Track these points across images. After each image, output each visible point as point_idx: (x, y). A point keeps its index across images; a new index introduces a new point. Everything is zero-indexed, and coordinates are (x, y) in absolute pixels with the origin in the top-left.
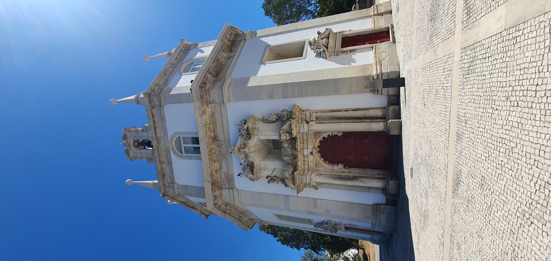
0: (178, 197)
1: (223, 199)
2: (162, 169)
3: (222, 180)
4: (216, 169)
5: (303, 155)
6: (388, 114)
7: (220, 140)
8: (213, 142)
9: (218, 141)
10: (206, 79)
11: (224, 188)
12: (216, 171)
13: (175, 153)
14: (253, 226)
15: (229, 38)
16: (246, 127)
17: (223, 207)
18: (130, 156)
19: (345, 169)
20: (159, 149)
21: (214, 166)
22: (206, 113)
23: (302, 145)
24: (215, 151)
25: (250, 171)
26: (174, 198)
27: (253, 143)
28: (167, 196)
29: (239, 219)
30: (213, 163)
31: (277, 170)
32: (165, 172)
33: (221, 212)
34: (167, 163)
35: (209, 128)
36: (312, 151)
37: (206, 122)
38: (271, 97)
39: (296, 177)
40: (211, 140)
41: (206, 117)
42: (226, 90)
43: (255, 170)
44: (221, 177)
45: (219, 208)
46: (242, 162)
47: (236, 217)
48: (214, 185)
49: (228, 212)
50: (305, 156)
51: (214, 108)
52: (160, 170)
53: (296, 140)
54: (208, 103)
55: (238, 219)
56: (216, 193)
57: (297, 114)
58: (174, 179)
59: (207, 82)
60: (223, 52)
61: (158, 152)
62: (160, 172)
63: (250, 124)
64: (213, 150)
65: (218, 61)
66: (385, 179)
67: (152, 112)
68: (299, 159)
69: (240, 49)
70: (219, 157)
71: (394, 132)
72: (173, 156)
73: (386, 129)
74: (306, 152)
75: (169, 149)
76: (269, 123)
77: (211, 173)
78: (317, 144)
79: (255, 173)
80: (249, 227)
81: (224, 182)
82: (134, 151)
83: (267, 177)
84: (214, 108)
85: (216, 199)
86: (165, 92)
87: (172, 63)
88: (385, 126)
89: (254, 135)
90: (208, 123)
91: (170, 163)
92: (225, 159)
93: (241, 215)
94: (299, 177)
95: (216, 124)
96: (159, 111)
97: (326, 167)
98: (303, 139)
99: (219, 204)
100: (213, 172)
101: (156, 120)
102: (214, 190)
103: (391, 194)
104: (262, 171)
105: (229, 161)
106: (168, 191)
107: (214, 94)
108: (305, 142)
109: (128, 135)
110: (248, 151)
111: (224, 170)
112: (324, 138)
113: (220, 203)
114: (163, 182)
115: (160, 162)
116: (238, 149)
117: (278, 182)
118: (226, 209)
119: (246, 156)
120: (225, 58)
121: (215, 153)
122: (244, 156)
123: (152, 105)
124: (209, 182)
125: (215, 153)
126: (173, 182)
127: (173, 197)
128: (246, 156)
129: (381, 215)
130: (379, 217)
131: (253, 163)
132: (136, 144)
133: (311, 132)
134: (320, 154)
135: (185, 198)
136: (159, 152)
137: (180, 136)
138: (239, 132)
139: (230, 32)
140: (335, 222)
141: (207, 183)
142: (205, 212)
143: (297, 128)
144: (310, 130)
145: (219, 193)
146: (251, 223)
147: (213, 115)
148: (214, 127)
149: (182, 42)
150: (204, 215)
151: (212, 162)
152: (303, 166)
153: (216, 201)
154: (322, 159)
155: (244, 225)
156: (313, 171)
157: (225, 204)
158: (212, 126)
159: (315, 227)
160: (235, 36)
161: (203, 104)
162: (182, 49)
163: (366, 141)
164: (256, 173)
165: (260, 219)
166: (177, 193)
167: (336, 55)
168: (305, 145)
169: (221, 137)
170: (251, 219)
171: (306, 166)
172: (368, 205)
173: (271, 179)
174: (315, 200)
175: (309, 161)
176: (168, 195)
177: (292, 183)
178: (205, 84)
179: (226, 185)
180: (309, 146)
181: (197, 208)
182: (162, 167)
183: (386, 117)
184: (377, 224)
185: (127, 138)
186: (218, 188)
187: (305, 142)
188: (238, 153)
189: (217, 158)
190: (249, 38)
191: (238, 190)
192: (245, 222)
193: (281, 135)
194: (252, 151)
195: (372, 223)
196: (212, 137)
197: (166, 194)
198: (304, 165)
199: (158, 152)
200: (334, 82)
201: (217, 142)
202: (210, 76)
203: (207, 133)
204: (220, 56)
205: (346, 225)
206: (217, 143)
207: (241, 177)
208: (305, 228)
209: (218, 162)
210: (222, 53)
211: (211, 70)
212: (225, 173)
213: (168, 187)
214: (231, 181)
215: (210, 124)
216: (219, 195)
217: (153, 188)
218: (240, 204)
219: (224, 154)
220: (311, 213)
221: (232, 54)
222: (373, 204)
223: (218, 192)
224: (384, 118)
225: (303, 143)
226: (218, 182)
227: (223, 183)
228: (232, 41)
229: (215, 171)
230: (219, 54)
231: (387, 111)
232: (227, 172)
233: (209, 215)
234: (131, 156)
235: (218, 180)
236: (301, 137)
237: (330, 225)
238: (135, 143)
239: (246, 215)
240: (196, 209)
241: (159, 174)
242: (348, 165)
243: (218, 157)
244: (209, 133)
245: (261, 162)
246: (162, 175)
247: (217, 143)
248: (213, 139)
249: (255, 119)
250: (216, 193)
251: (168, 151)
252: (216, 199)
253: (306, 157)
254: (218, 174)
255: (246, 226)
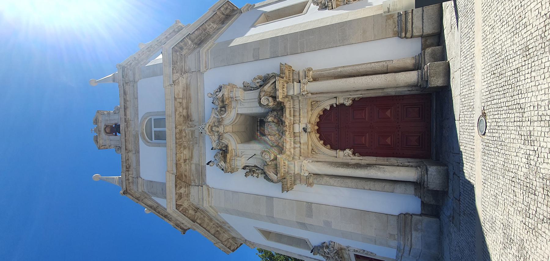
0: (145, 198)
1: (191, 200)
2: (128, 160)
3: (192, 174)
4: (185, 157)
5: (293, 133)
6: (423, 61)
7: (193, 119)
8: (185, 122)
9: (191, 121)
10: (184, 44)
11: (193, 185)
12: (185, 161)
13: (144, 138)
14: (237, 249)
15: (223, 12)
16: (220, 95)
17: (191, 212)
18: (99, 143)
19: (355, 156)
20: (127, 134)
21: (182, 154)
22: (179, 84)
23: (292, 118)
24: (186, 134)
25: (222, 158)
26: (139, 199)
27: (230, 116)
28: (130, 194)
29: (216, 235)
30: (182, 149)
31: (258, 157)
32: (130, 163)
33: (187, 218)
34: (134, 152)
35: (180, 103)
36: (306, 126)
37: (178, 94)
38: (257, 59)
39: (279, 163)
40: (182, 119)
41: (179, 89)
42: (204, 53)
43: (228, 156)
44: (190, 169)
45: (184, 212)
46: (214, 145)
47: (211, 231)
48: (180, 180)
49: (198, 221)
50: (295, 135)
51: (189, 79)
52: (125, 160)
53: (284, 110)
54: (184, 72)
55: (215, 234)
56: (182, 191)
57: (287, 73)
58: (139, 173)
59: (185, 48)
60: (213, 23)
61: (125, 137)
62: (125, 162)
63: (225, 92)
64: (184, 133)
65: (205, 30)
66: (420, 167)
67: (124, 88)
68: (288, 139)
69: (233, 20)
70: (191, 142)
71: (437, 82)
72: (141, 142)
73: (422, 78)
74: (298, 128)
75: (138, 134)
76: (251, 90)
77: (178, 163)
78: (315, 119)
79: (229, 161)
80: (230, 249)
81: (193, 176)
82: (104, 138)
83: (244, 168)
84: (190, 78)
85: (181, 198)
86: (141, 65)
87: (160, 41)
88: (420, 74)
89: (231, 107)
90: (181, 96)
91: (137, 152)
92: (197, 145)
93: (218, 229)
94: (284, 163)
95: (190, 99)
96: (133, 87)
97: (327, 152)
98: (294, 110)
99: (184, 206)
100: (181, 161)
101: (128, 99)
102: (178, 186)
103: (432, 190)
104: (238, 158)
105: (201, 147)
106: (131, 188)
107: (191, 62)
108: (297, 114)
109: (100, 119)
110: (222, 130)
111: (195, 160)
112: (325, 111)
113: (186, 205)
114: (126, 176)
115: (126, 149)
116: (210, 127)
117: (258, 175)
118: (196, 217)
119: (220, 137)
120: (215, 29)
121: (185, 137)
122: (217, 137)
123: (126, 80)
124: (173, 174)
125: (185, 137)
126: (138, 176)
127: (138, 197)
128: (220, 137)
129: (413, 232)
130: (409, 237)
131: (227, 146)
132: (108, 130)
133: (303, 93)
134: (318, 135)
135: (153, 200)
136: (126, 138)
137: (151, 118)
138: (212, 103)
139: (225, 6)
140: (341, 245)
141: (171, 174)
142: (182, 225)
143: (285, 89)
144: (302, 90)
145: (185, 191)
146: (234, 243)
147: (187, 87)
148: (187, 103)
149: (176, 23)
150: (180, 228)
151: (180, 148)
152: (292, 151)
153: (180, 201)
154: (322, 142)
155: (223, 245)
156: (307, 157)
157: (194, 208)
158: (184, 101)
159: (311, 252)
160: (231, 11)
161: (175, 71)
162: (176, 30)
163: (388, 113)
164: (230, 160)
165: (244, 238)
166: (140, 190)
167: (345, 3)
168: (297, 118)
169: (195, 117)
170: (234, 238)
171: (296, 149)
172: (392, 215)
173: (250, 170)
174: (309, 205)
175: (302, 142)
176: (132, 194)
177: (274, 172)
178: (181, 48)
179: (196, 181)
180: (302, 119)
181: (171, 218)
182: (128, 156)
183: (420, 65)
184: (407, 248)
185: (98, 122)
186: (186, 183)
187: (297, 114)
188: (209, 132)
189: (188, 144)
190: (245, 10)
191: (209, 187)
192: (224, 240)
193: (260, 99)
194: (228, 130)
195: (398, 249)
196: (183, 116)
197: (129, 192)
198: (294, 148)
199: (125, 137)
200: (341, 28)
201: (190, 123)
202: (190, 42)
203: (177, 109)
204: (209, 26)
205: (357, 251)
206: (189, 124)
207: (211, 166)
208: (300, 255)
209: (189, 148)
210: (212, 24)
211: (193, 37)
212: (196, 165)
213: (133, 182)
214: (201, 175)
215: (182, 99)
216: (185, 194)
217: (118, 185)
218: (211, 208)
219: (197, 138)
220: (303, 226)
221: (224, 25)
222: (400, 214)
223: (185, 190)
224: (417, 67)
225: (294, 116)
226: (185, 176)
227: (192, 178)
228: (227, 15)
229: (183, 161)
230: (208, 23)
231: (423, 59)
232: (198, 163)
233: (186, 230)
234: (100, 143)
235: (187, 174)
236: (292, 106)
237: (332, 249)
238: (106, 129)
239: (225, 231)
240: (170, 219)
241: (122, 165)
242: (359, 150)
243: (189, 143)
244: (181, 110)
245: (238, 145)
246: (126, 166)
247: (189, 124)
248: (185, 118)
249: (233, 86)
250: (182, 191)
251: (136, 137)
252: (180, 199)
253: (298, 136)
254: (187, 165)
255: (224, 244)
